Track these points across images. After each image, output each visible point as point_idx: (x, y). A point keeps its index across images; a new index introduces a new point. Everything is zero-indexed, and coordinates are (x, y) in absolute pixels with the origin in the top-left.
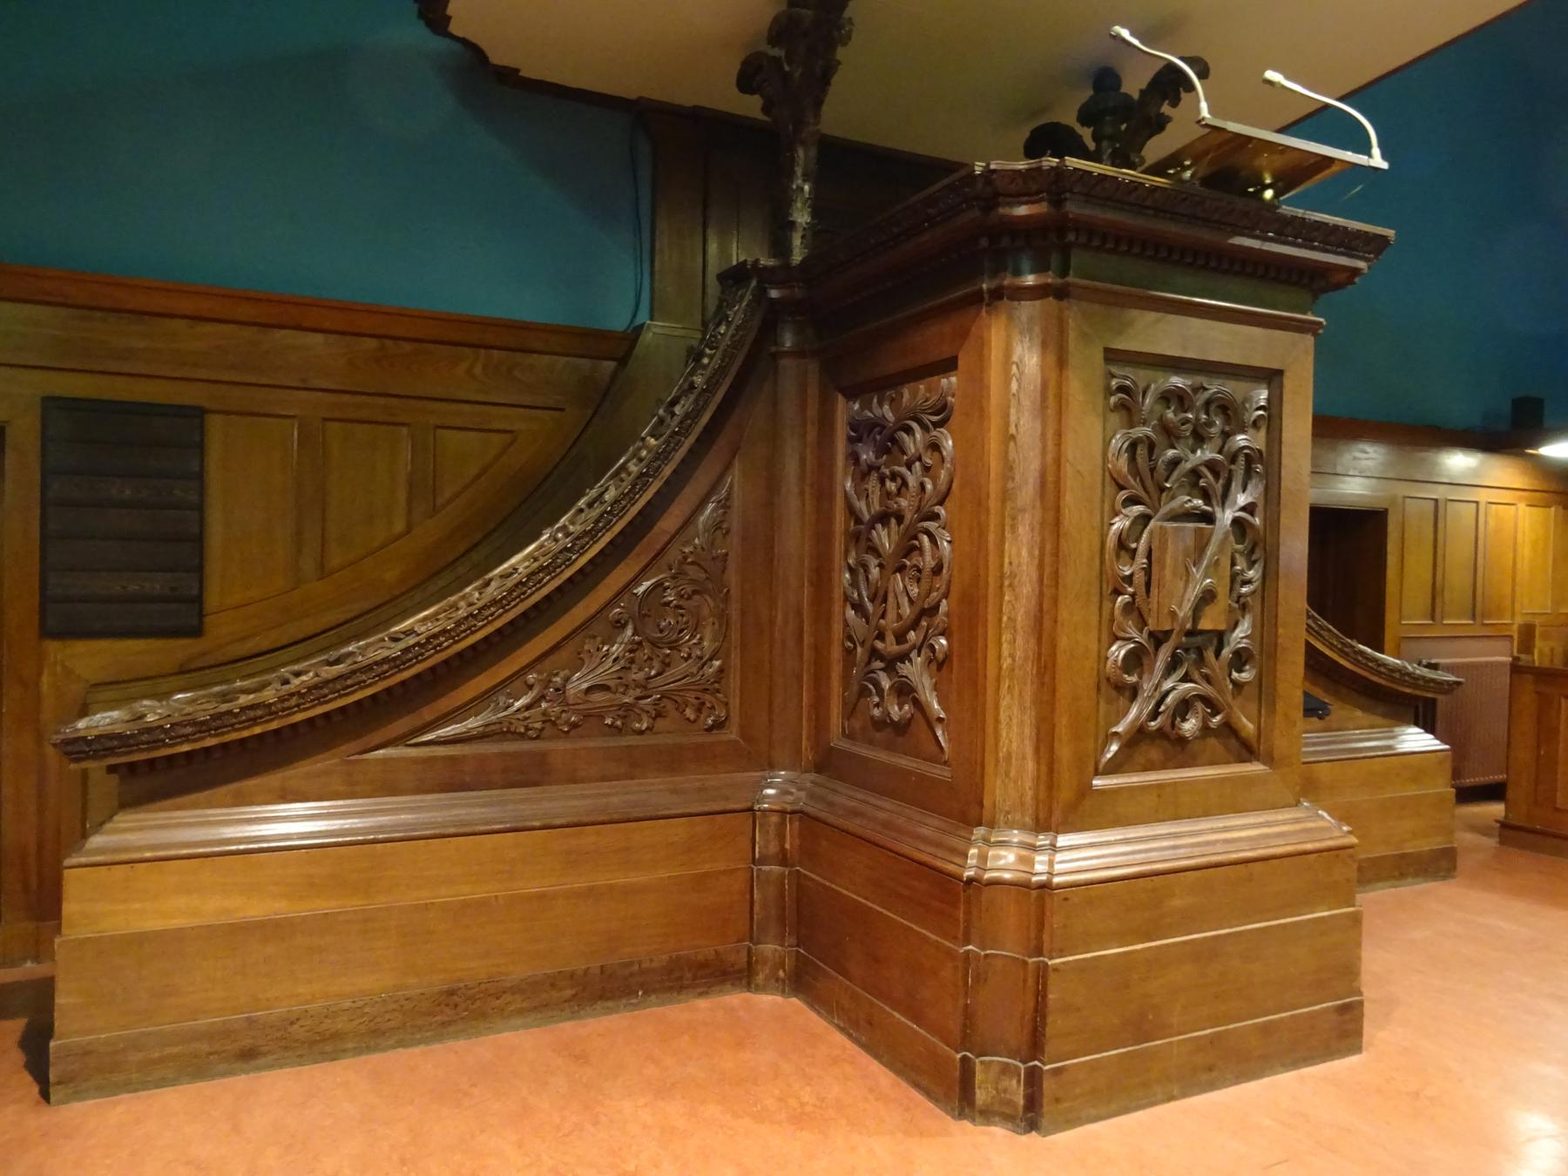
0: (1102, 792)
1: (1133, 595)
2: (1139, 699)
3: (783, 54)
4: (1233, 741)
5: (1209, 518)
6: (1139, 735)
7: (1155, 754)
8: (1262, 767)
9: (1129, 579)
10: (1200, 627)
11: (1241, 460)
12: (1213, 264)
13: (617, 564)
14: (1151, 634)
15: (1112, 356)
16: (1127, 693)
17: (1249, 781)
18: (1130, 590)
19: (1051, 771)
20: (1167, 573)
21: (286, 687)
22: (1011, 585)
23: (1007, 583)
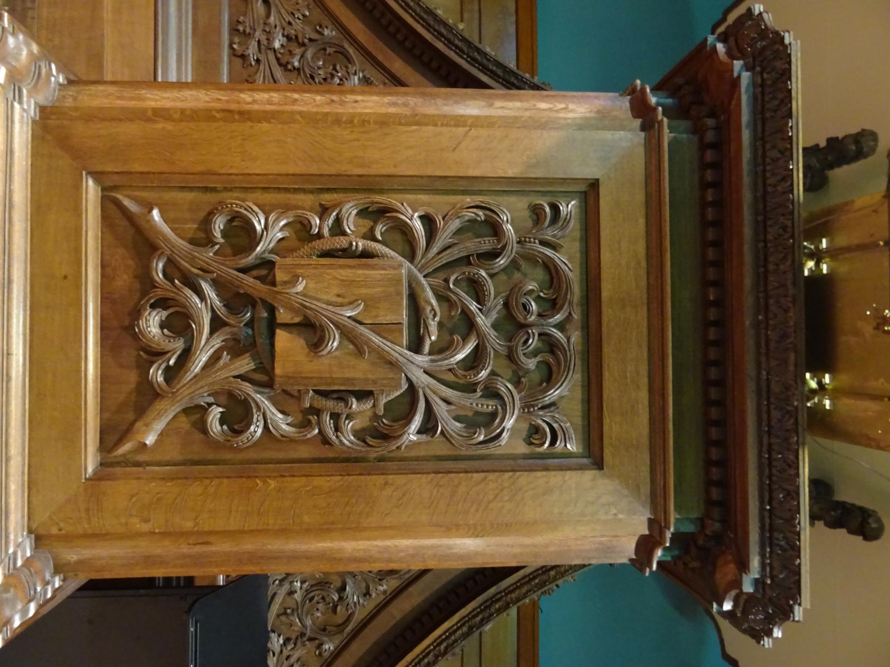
0: (77, 187)
1: (319, 236)
3: (668, 545)
5: (416, 346)
6: (145, 244)
7: (124, 280)
8: (90, 470)
9: (338, 229)
10: (278, 331)
11: (489, 406)
13: (365, 25)
14: (269, 265)
15: (590, 192)
18: (326, 232)
19: (113, 119)
20: (345, 271)
22: (333, 101)
23: (335, 98)
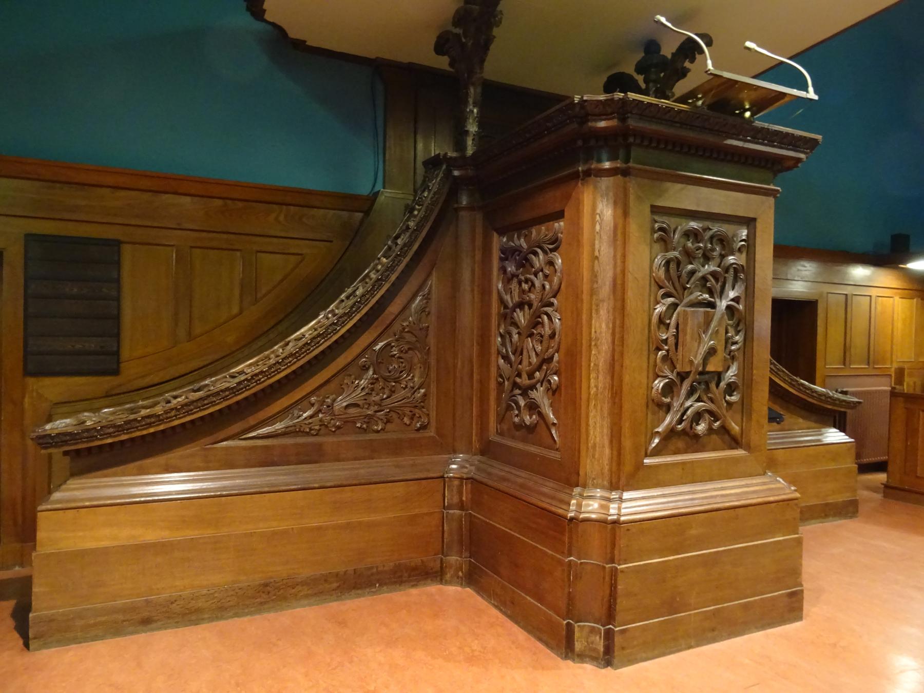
0: (649, 467)
1: (668, 351)
2: (671, 412)
4: (727, 437)
5: (712, 305)
6: (671, 433)
7: (680, 444)
8: (744, 452)
9: (665, 341)
10: (707, 369)
11: (732, 271)
12: (715, 155)
13: (364, 332)
14: (678, 374)
15: (655, 210)
16: (664, 409)
17: (736, 460)
18: (666, 347)
19: (619, 454)
20: (688, 338)
21: (169, 405)
22: (595, 345)
23: (593, 343)
